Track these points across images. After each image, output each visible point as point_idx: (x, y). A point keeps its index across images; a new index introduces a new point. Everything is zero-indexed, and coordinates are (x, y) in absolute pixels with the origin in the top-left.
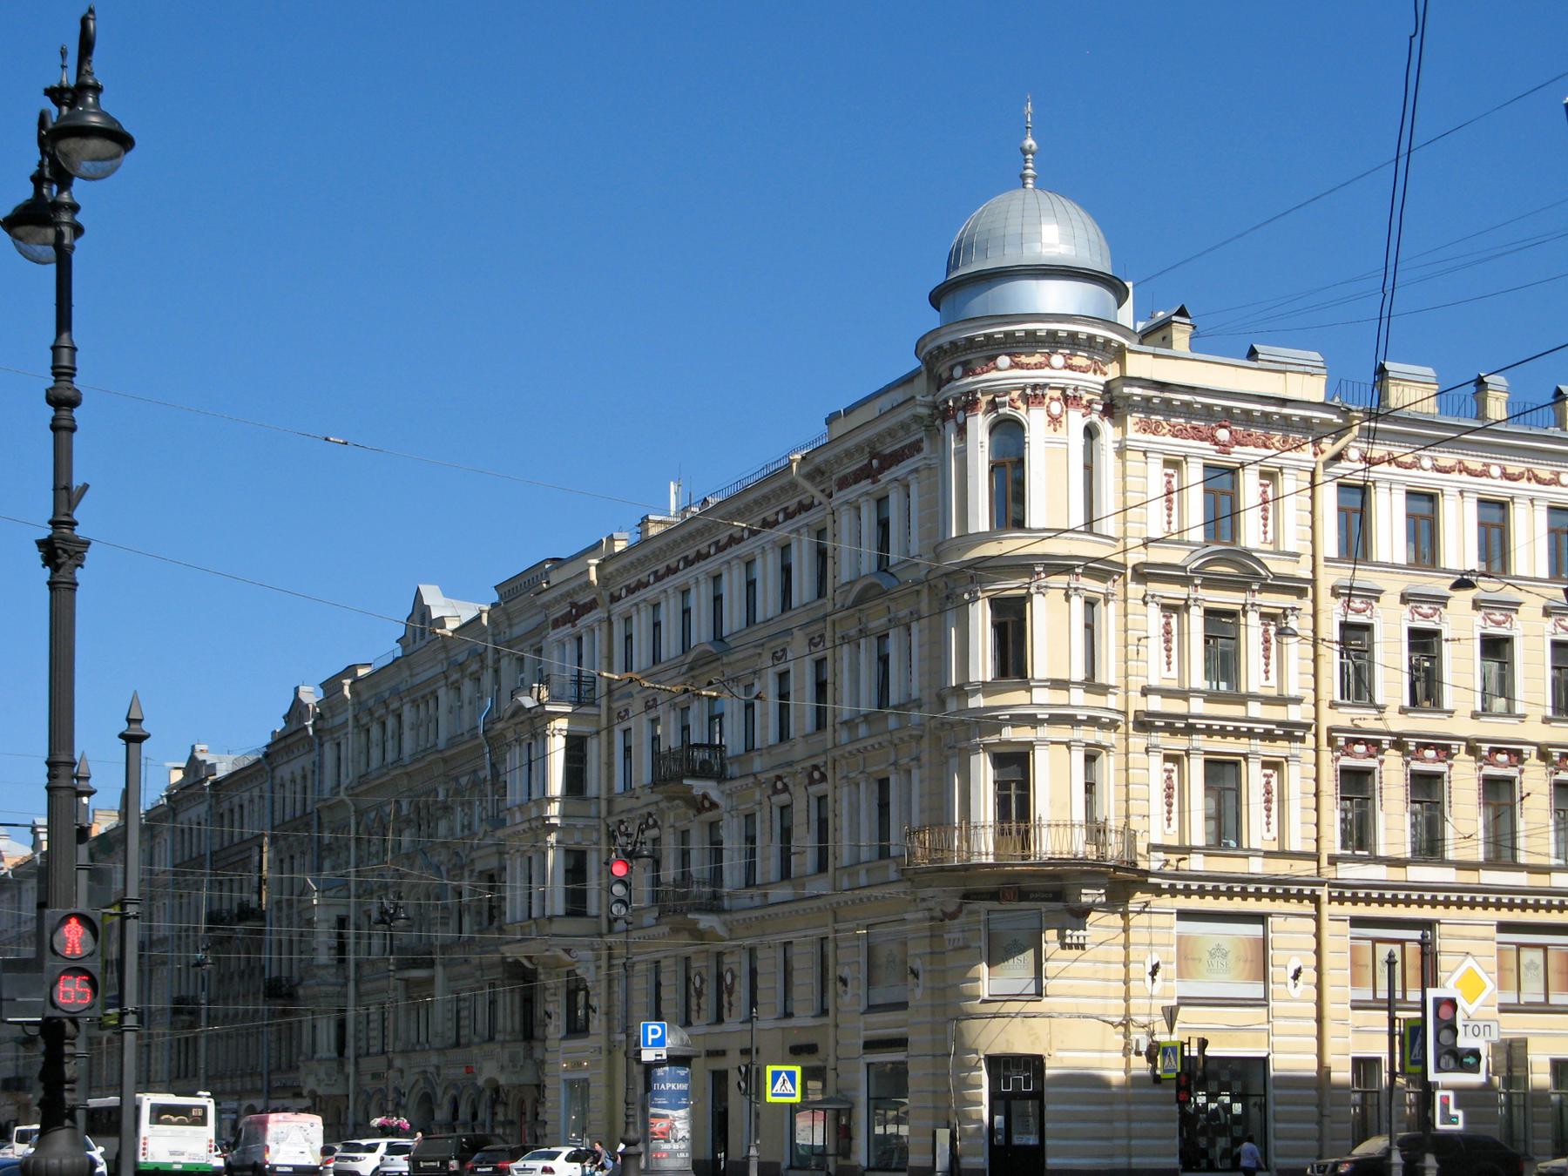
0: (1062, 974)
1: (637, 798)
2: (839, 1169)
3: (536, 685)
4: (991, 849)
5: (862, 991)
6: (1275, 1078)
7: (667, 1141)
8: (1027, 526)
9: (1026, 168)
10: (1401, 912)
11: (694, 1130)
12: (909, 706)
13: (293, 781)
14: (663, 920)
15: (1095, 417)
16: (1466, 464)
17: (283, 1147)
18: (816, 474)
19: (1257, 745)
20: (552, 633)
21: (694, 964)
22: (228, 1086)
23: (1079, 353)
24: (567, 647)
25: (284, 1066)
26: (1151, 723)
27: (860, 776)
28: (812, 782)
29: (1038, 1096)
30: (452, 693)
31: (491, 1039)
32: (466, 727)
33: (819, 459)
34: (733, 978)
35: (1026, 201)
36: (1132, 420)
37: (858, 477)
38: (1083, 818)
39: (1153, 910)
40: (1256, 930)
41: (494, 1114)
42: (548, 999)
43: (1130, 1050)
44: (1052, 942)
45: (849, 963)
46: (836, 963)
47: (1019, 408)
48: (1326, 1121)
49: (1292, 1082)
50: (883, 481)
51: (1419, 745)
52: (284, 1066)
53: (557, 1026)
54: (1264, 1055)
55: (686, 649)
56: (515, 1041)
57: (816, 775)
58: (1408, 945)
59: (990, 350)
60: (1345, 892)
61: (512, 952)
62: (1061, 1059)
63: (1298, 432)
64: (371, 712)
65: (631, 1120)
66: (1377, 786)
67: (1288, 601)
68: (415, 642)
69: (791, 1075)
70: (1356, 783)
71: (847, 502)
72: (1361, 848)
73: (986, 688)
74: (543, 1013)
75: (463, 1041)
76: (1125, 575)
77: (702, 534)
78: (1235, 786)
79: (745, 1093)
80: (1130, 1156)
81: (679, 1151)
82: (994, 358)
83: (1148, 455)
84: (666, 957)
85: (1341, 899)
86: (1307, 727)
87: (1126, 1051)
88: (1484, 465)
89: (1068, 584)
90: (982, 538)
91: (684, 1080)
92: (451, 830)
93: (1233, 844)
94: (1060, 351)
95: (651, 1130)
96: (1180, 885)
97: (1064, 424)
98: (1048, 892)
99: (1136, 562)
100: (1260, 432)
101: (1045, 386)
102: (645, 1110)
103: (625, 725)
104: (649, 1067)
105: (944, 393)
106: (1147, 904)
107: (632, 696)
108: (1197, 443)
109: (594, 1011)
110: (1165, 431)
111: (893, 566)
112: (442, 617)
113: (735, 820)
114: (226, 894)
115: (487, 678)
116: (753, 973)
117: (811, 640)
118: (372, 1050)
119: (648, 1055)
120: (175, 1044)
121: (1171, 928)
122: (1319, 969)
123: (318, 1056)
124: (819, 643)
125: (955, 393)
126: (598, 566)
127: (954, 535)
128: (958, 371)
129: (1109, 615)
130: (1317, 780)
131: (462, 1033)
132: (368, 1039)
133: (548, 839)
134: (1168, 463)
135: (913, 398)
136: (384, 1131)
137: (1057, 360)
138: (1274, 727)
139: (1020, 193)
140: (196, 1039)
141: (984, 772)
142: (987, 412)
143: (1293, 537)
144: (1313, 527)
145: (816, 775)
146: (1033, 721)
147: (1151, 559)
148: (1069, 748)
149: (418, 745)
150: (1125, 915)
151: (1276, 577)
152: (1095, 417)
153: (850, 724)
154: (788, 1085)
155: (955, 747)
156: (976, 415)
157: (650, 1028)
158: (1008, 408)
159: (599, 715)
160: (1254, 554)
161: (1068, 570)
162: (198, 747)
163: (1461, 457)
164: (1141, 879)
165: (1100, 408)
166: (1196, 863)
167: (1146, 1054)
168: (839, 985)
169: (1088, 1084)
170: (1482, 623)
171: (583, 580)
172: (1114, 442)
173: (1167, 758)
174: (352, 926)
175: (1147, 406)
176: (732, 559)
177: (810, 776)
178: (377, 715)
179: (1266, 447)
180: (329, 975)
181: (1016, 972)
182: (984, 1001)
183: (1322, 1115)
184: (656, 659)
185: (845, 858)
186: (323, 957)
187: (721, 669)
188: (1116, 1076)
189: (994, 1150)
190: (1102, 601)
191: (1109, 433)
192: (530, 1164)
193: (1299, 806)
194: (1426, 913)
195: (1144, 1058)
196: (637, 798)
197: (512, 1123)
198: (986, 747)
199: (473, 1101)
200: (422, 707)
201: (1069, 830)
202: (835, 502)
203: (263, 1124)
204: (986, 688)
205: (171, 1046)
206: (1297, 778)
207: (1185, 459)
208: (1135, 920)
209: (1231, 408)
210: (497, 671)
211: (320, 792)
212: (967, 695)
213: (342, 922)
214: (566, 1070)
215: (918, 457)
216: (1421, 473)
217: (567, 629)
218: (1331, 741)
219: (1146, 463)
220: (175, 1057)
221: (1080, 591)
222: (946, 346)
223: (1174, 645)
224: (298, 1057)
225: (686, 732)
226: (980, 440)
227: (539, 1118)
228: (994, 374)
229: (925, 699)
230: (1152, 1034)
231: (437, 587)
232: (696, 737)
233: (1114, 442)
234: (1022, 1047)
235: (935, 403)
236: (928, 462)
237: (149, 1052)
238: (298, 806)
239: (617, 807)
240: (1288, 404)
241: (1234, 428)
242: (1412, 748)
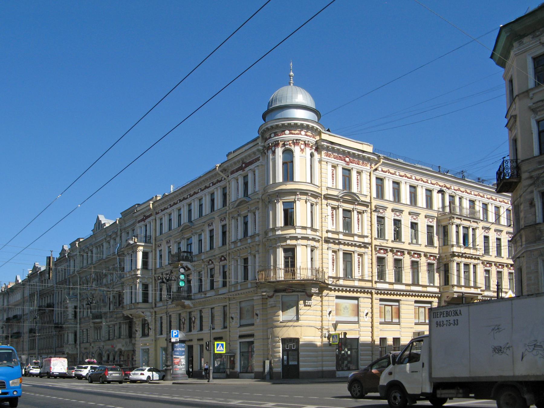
0: (305, 314)
1: (164, 269)
2: (230, 372)
3: (134, 237)
4: (283, 276)
5: (238, 321)
6: (361, 344)
7: (179, 365)
8: (294, 181)
9: (290, 81)
10: (392, 297)
11: (186, 362)
12: (255, 236)
13: (62, 271)
14: (174, 302)
16: (407, 175)
17: (56, 367)
18: (224, 170)
20: (138, 224)
21: (182, 315)
22: (44, 352)
24: (142, 228)
25: (59, 346)
27: (238, 257)
28: (221, 260)
29: (297, 350)
30: (107, 244)
31: (120, 338)
32: (112, 252)
33: (225, 165)
34: (185, 320)
36: (323, 153)
37: (237, 170)
38: (310, 267)
40: (355, 302)
41: (120, 358)
42: (137, 326)
43: (323, 336)
44: (302, 304)
45: (234, 312)
46: (230, 313)
48: (374, 355)
49: (365, 345)
51: (396, 251)
52: (59, 346)
53: (139, 334)
54: (358, 337)
55: (180, 225)
56: (127, 338)
57: (223, 258)
58: (393, 307)
59: (283, 128)
60: (379, 291)
61: (126, 313)
62: (304, 339)
63: (366, 161)
64: (84, 250)
65: (168, 359)
66: (386, 262)
67: (364, 208)
68: (97, 230)
69: (222, 345)
70: (381, 261)
71: (234, 178)
72: (381, 280)
73: (281, 229)
74: (135, 331)
75: (110, 339)
76: (321, 197)
77: (186, 192)
78: (350, 260)
79: (208, 350)
80: (323, 367)
81: (182, 368)
82: (284, 131)
83: (328, 163)
84: (173, 314)
85: (377, 293)
87: (322, 337)
88: (411, 176)
90: (280, 184)
91: (183, 347)
92: (107, 281)
93: (350, 277)
94: (304, 130)
95: (174, 362)
96: (337, 288)
97: (305, 152)
100: (357, 160)
102: (172, 356)
103: (160, 249)
104: (173, 344)
106: (328, 293)
107: (162, 240)
109: (151, 329)
112: (105, 223)
113: (196, 273)
114: (35, 287)
115: (118, 239)
116: (201, 317)
117: (221, 219)
118: (84, 342)
119: (173, 340)
120: (30, 341)
121: (334, 301)
122: (372, 312)
123: (69, 343)
124: (224, 220)
125: (272, 141)
126: (152, 204)
127: (271, 183)
128: (273, 135)
129: (317, 208)
130: (372, 259)
131: (110, 336)
132: (83, 339)
133: (137, 281)
134: (333, 166)
135: (258, 143)
136: (89, 363)
138: (361, 244)
140: (35, 339)
141: (281, 254)
142: (282, 147)
143: (365, 191)
144: (370, 188)
145: (223, 258)
146: (296, 238)
147: (329, 193)
148: (307, 247)
149: (97, 259)
150: (321, 297)
151: (362, 201)
152: (313, 151)
153: (235, 243)
154: (221, 348)
155: (271, 247)
157: (174, 332)
159: (152, 246)
160: (357, 195)
161: (306, 194)
162: (36, 263)
163: (406, 173)
164: (326, 286)
165: (315, 148)
166: (341, 282)
167: (327, 337)
168: (231, 319)
169: (311, 346)
170: (411, 218)
171: (148, 208)
172: (318, 159)
174: (78, 309)
175: (327, 149)
176: (195, 198)
177: (221, 259)
178: (86, 251)
179: (358, 164)
180: (72, 321)
181: (291, 314)
182: (281, 322)
183: (372, 354)
184: (170, 229)
185: (233, 281)
186: (71, 316)
187: (191, 230)
188: (319, 344)
189: (284, 366)
191: (317, 156)
192: (136, 372)
194: (398, 298)
195: (327, 338)
196: (164, 269)
197: (125, 361)
198: (282, 246)
199: (114, 355)
200: (99, 248)
201: (306, 270)
202: (229, 178)
203: (50, 361)
204: (281, 229)
205: (29, 341)
206: (367, 259)
208: (325, 298)
210: (121, 237)
211: (69, 273)
212: (276, 231)
213: (76, 307)
214: (142, 346)
215: (258, 162)
216: (396, 176)
217: (143, 223)
218: (375, 249)
220: (30, 344)
221: (310, 201)
222: (269, 127)
223: (334, 219)
224: (63, 343)
225: (179, 249)
227: (134, 359)
228: (284, 136)
229: (261, 233)
230: (329, 332)
231: (103, 216)
232: (183, 250)
233: (318, 159)
234: (293, 335)
237: (23, 343)
238: (63, 277)
239: (158, 272)
242: (395, 252)
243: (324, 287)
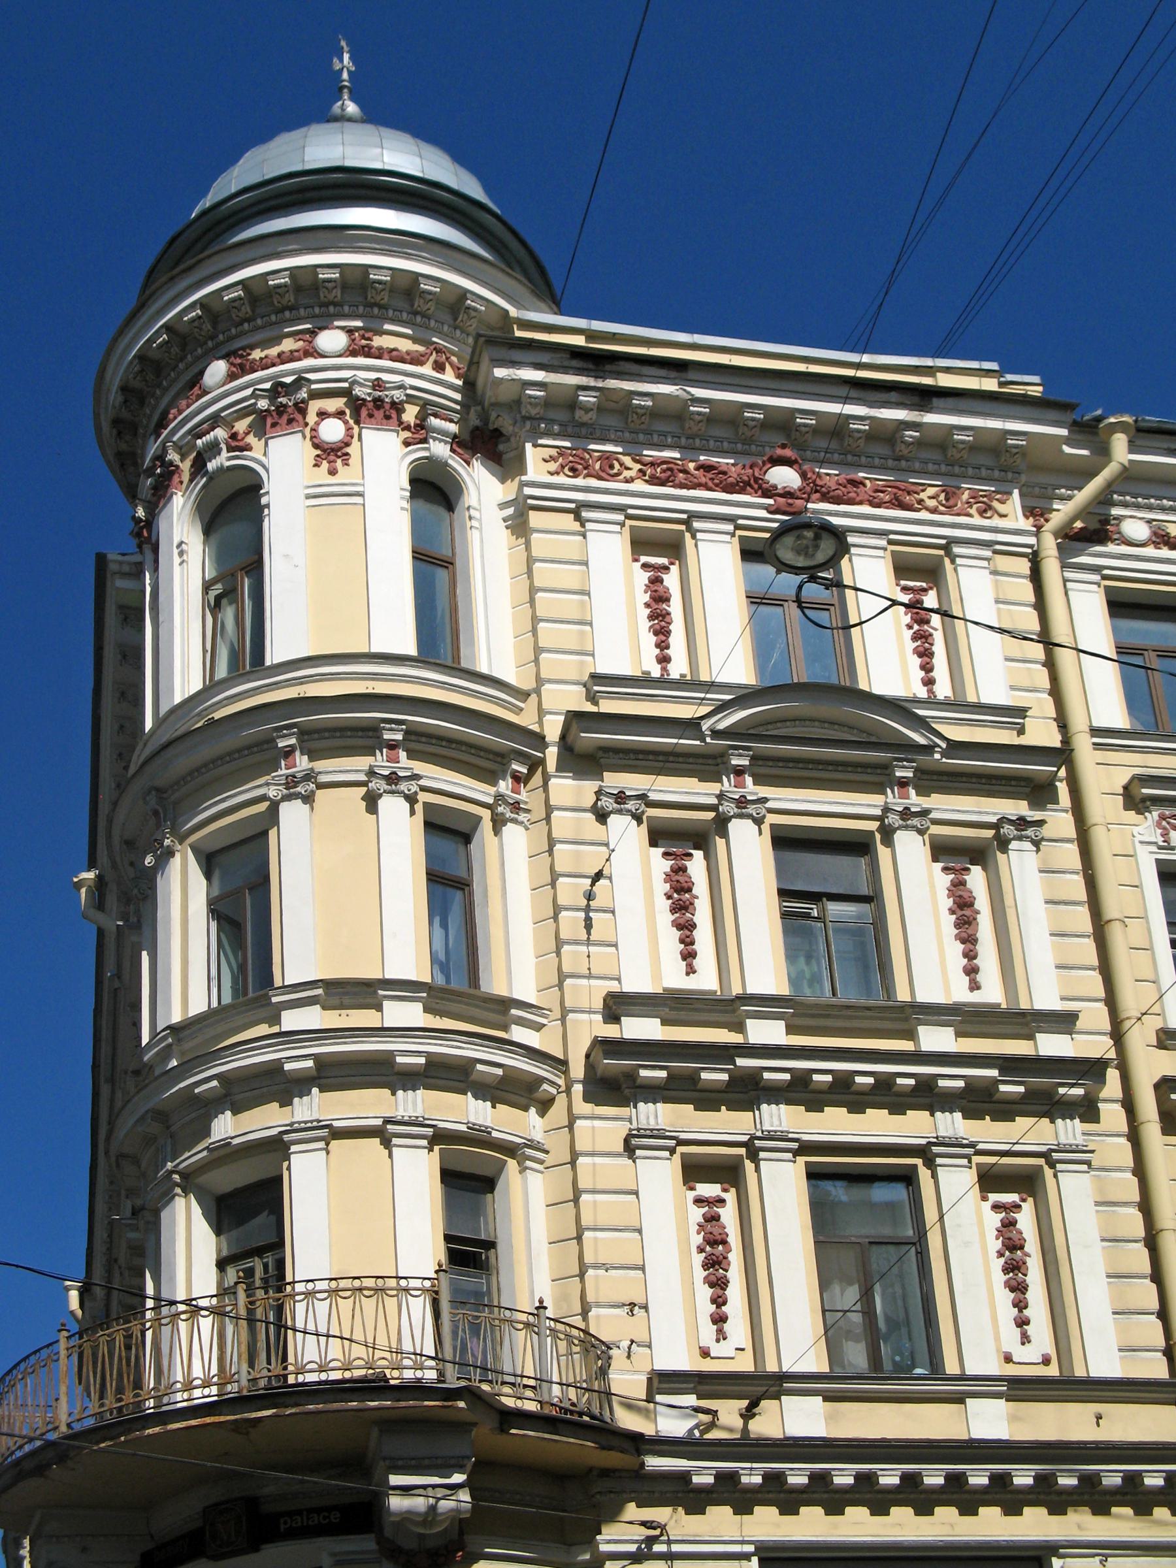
15: (440, 449)
19: (952, 1124)
23: (387, 327)
26: (631, 1076)
39: (676, 1548)
47: (248, 448)
86: (1092, 1069)
94: (336, 323)
97: (354, 460)
98: (330, 1509)
110: (632, 473)
134: (641, 544)
137: (332, 340)
148: (387, 1143)
151: (956, 748)
152: (440, 449)
158: (224, 454)
173: (694, 1172)
193: (1101, 1271)
207: (689, 528)
219: (585, 537)
233: (503, 506)
240: (936, 402)
243: (606, 1473)
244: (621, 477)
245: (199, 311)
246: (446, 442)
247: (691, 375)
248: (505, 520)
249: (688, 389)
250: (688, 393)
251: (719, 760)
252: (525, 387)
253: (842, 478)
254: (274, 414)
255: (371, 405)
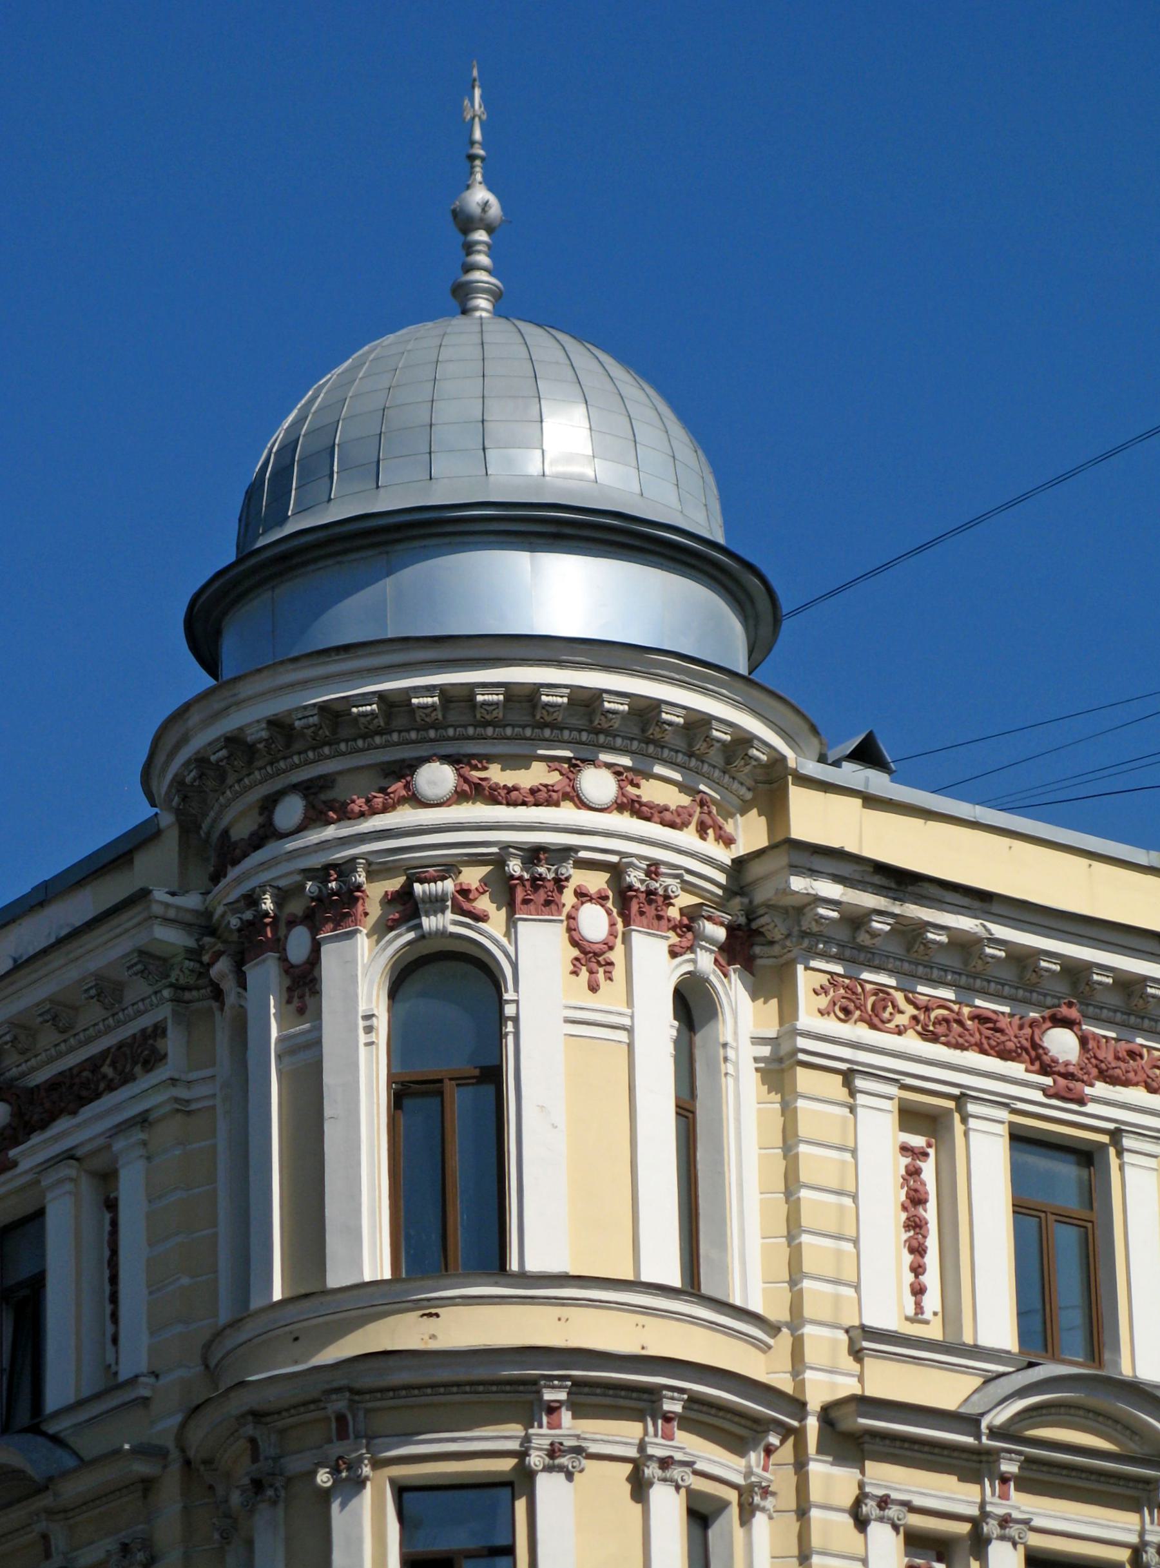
9: (469, 268)
23: (659, 769)
35: (487, 338)
47: (481, 918)
50: (24, 1165)
76: (799, 1434)
82: (406, 769)
83: (860, 1083)
89: (642, 1447)
94: (605, 757)
97: (619, 972)
99: (829, 1397)
101: (567, 852)
105: (246, 876)
108: (992, 1063)
111: (56, 1414)
125: (284, 874)
127: (277, 1295)
128: (290, 811)
135: (143, 894)
139: (459, 322)
147: (874, 1390)
152: (705, 961)
156: (351, 935)
165: (721, 933)
190: (734, 1510)
207: (960, 1108)
209: (1089, 967)
215: (146, 1081)
219: (852, 1109)
226: (363, 1008)
233: (758, 1041)
235: (208, 914)
236: (182, 1093)
241: (1087, 1028)
244: (891, 1025)
245: (436, 699)
246: (711, 951)
247: (996, 908)
248: (756, 1060)
249: (989, 925)
250: (988, 930)
251: (984, 1458)
252: (818, 903)
253: (1123, 1046)
254: (528, 884)
255: (642, 897)
